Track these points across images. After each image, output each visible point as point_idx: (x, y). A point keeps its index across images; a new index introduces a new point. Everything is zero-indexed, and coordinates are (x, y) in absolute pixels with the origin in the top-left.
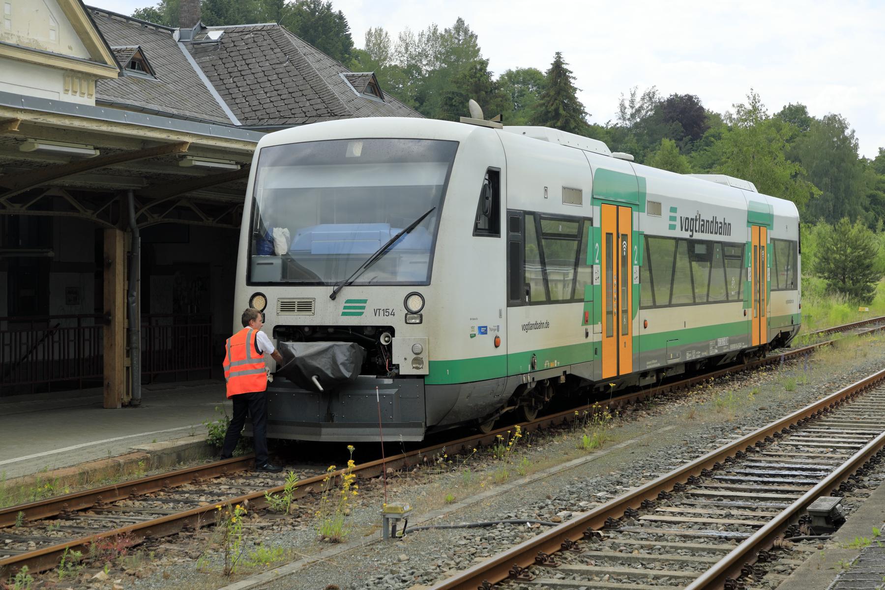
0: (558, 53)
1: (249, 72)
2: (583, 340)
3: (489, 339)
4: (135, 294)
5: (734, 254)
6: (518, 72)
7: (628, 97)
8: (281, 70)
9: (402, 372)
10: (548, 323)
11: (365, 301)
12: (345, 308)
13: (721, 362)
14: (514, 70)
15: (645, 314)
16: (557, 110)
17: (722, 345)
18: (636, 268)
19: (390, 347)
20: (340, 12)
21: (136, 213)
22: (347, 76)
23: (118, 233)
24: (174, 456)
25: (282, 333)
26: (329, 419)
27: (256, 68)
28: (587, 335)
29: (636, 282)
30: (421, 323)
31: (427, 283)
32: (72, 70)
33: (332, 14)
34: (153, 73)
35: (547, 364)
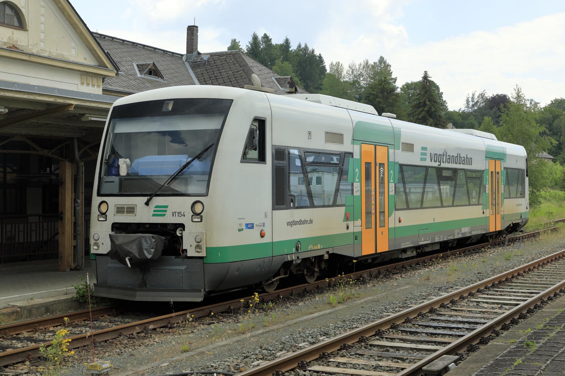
0: (425, 72)
1: (220, 77)
2: (345, 231)
3: (256, 232)
4: (79, 201)
5: (476, 177)
6: (412, 83)
7: (471, 96)
8: (237, 76)
9: (189, 254)
10: (311, 222)
11: (167, 207)
12: (166, 211)
13: (469, 242)
14: (410, 82)
15: (399, 214)
16: (425, 102)
17: (466, 231)
18: (502, 186)
19: (182, 237)
20: (320, 54)
21: (79, 151)
22: (276, 79)
23: (68, 164)
24: (43, 309)
25: (117, 227)
26: (143, 286)
27: (225, 75)
28: (348, 228)
29: (503, 192)
30: (201, 221)
31: (206, 195)
32: (85, 72)
33: (315, 55)
34: (162, 77)
35: (311, 247)
